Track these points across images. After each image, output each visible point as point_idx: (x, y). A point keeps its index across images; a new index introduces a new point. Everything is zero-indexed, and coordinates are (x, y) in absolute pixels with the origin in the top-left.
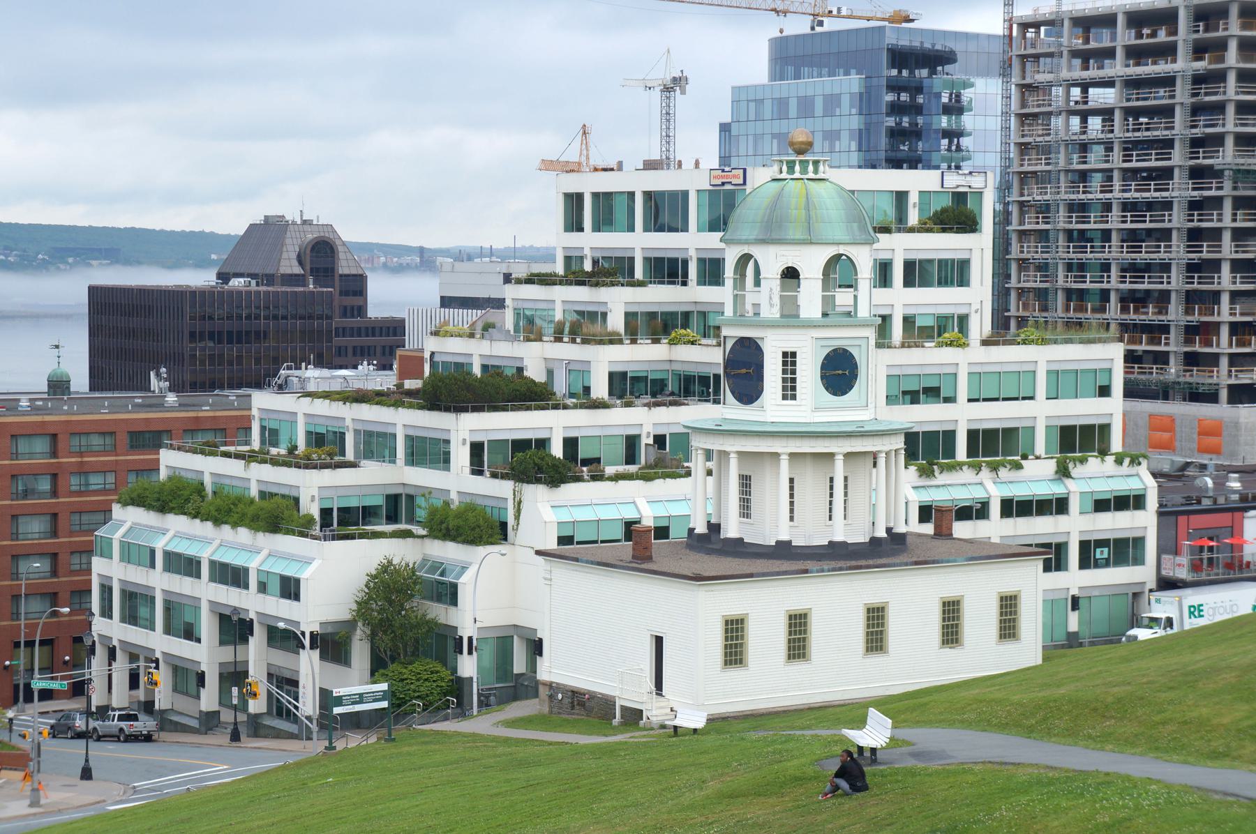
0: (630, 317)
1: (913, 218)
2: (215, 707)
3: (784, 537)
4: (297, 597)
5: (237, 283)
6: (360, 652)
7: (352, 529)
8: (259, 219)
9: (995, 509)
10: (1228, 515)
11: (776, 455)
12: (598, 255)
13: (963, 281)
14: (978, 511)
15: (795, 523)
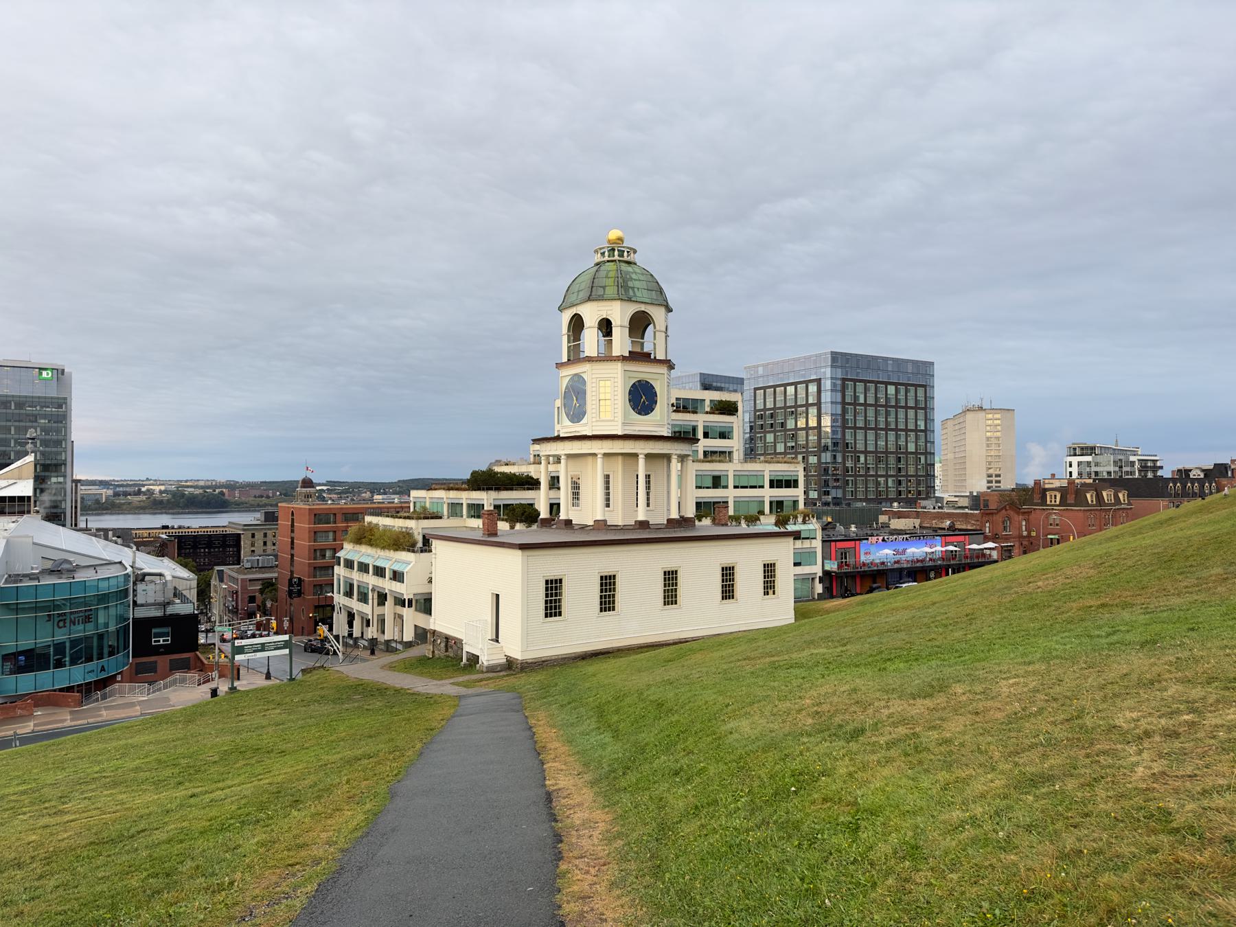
15: (651, 508)
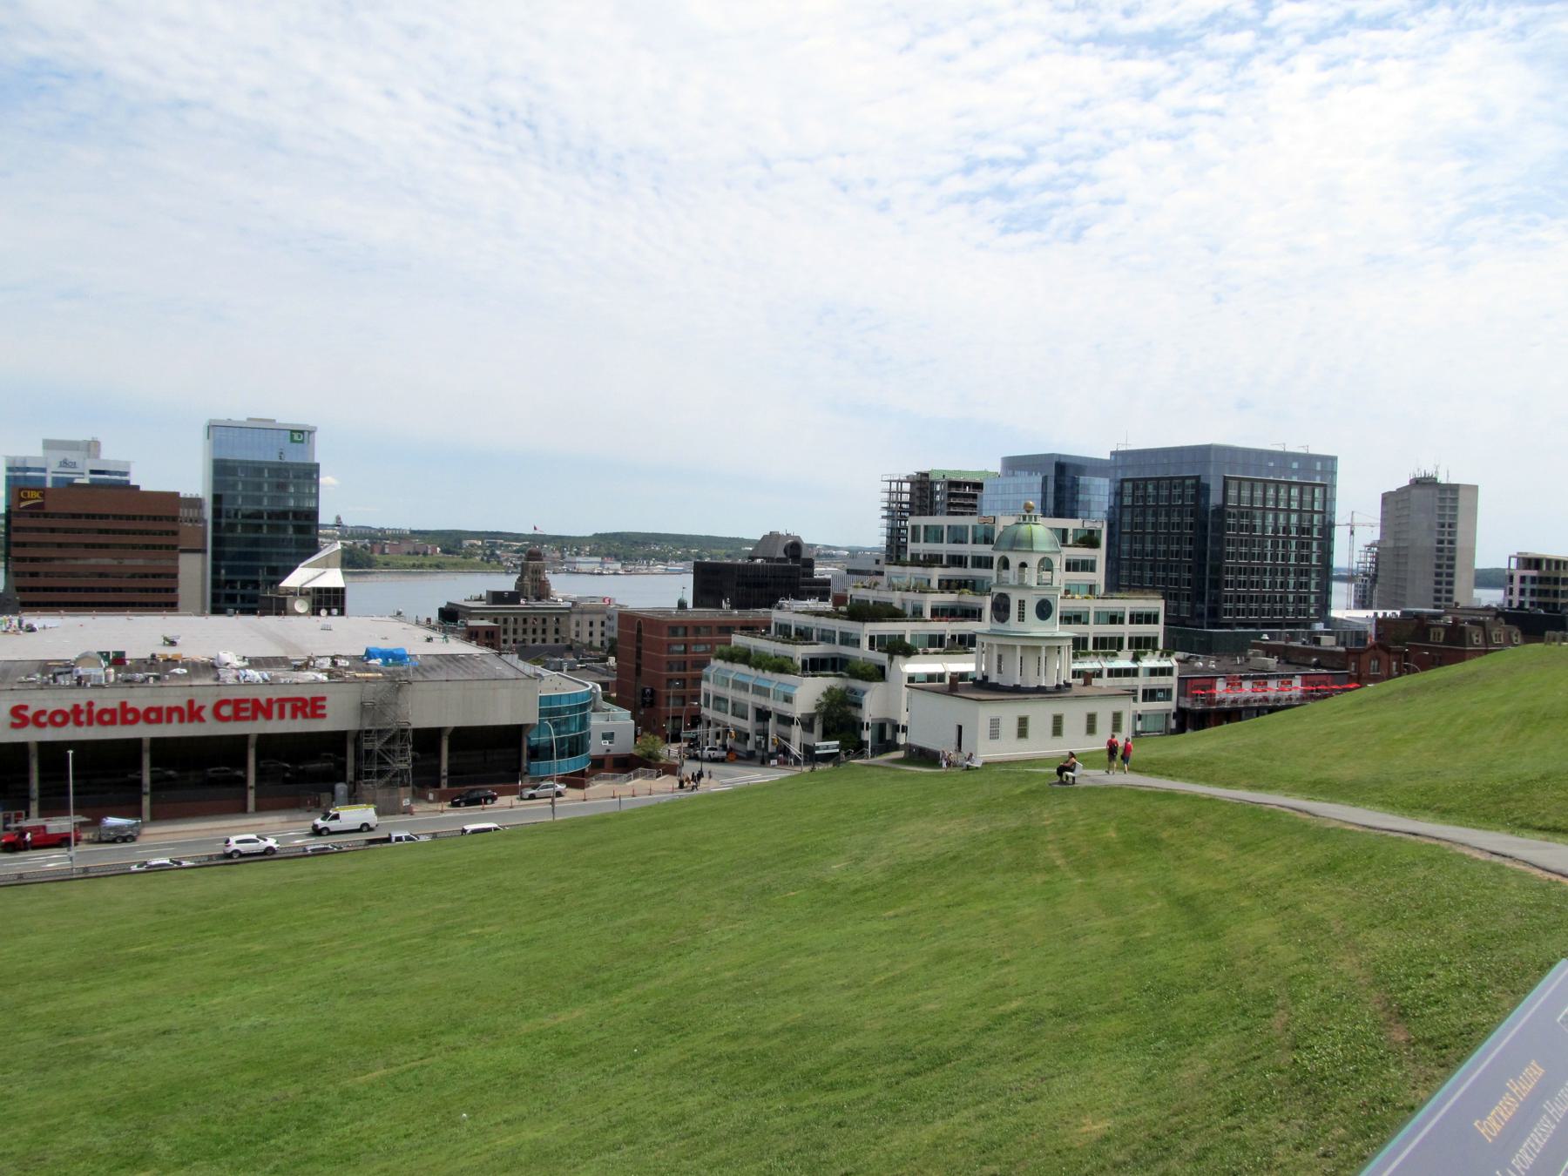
0: (940, 581)
1: (1070, 541)
2: (753, 749)
3: (1018, 683)
4: (791, 702)
5: (759, 561)
6: (818, 728)
7: (816, 673)
8: (768, 533)
9: (1105, 674)
10: (1209, 680)
11: (1014, 647)
12: (927, 553)
13: (1093, 569)
14: (1099, 674)
